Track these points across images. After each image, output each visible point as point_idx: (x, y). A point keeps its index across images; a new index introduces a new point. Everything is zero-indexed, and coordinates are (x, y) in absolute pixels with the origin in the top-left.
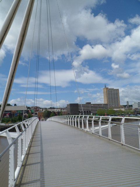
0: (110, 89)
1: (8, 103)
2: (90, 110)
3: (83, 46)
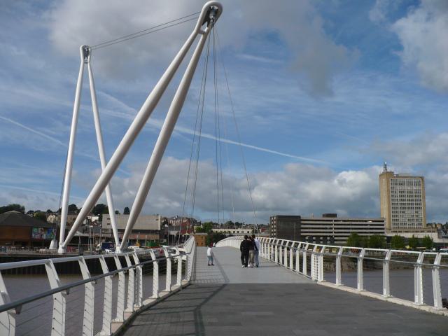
0: (397, 176)
2: (333, 234)
3: (400, 18)
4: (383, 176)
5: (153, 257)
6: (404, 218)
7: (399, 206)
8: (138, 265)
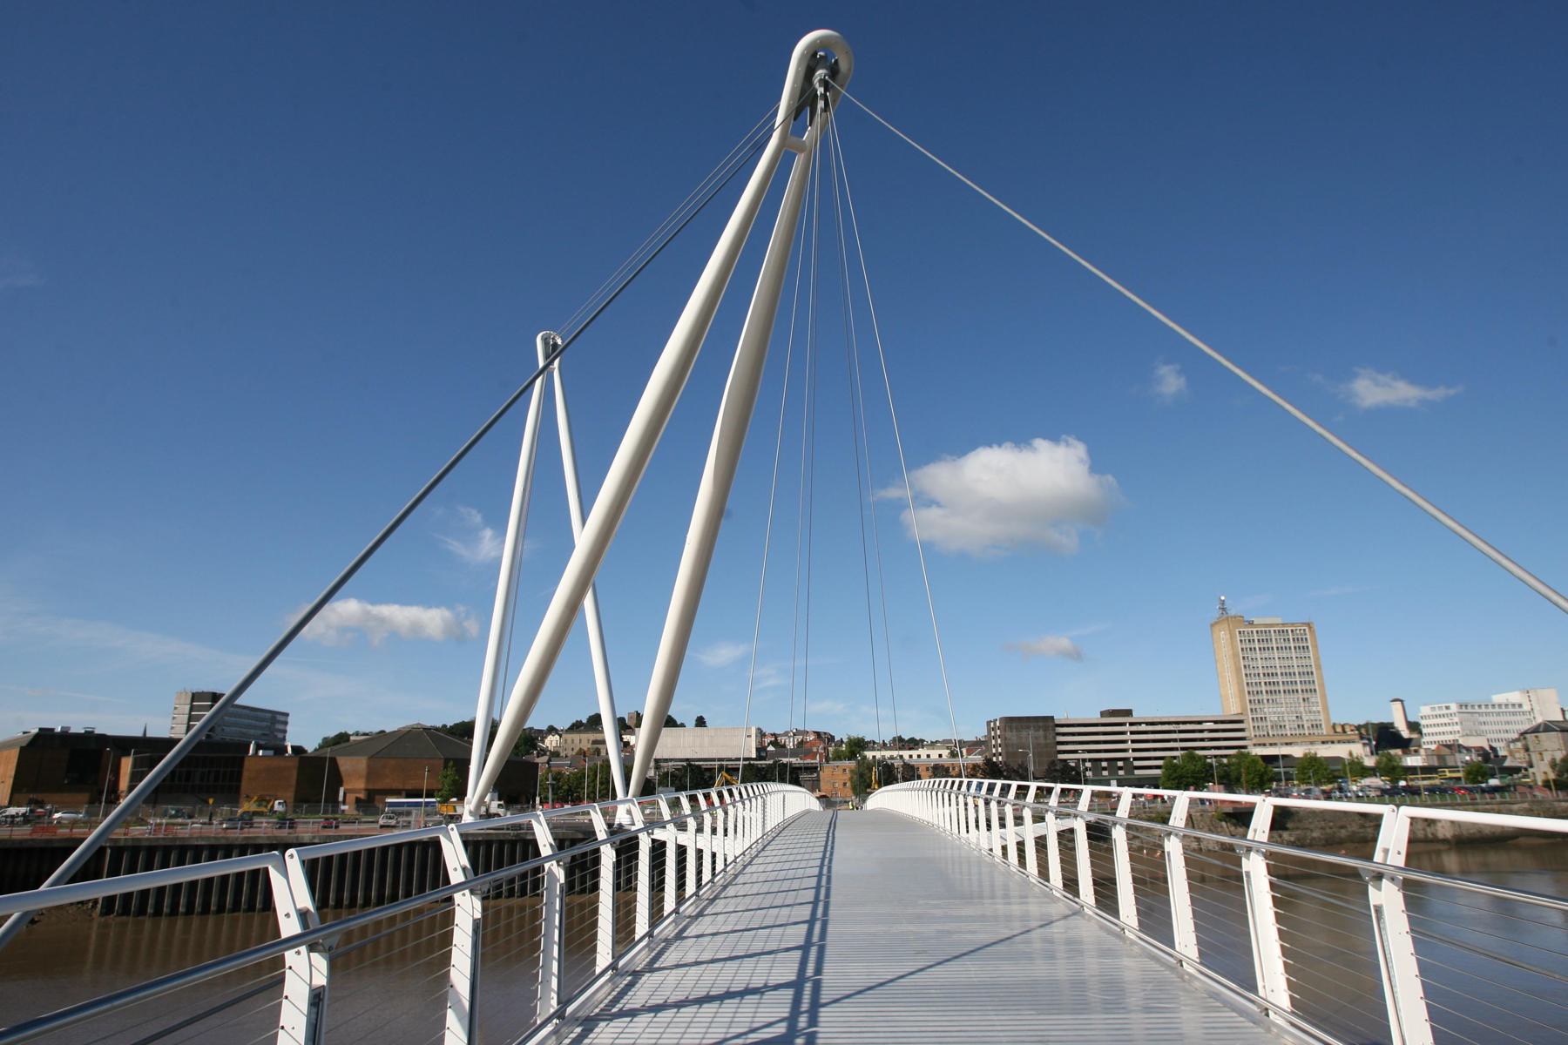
1: (790, 992)
4: (1217, 628)
5: (544, 839)
6: (1279, 711)
7: (1264, 688)
8: (548, 858)
